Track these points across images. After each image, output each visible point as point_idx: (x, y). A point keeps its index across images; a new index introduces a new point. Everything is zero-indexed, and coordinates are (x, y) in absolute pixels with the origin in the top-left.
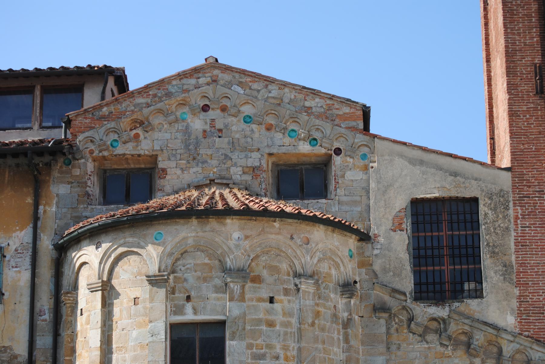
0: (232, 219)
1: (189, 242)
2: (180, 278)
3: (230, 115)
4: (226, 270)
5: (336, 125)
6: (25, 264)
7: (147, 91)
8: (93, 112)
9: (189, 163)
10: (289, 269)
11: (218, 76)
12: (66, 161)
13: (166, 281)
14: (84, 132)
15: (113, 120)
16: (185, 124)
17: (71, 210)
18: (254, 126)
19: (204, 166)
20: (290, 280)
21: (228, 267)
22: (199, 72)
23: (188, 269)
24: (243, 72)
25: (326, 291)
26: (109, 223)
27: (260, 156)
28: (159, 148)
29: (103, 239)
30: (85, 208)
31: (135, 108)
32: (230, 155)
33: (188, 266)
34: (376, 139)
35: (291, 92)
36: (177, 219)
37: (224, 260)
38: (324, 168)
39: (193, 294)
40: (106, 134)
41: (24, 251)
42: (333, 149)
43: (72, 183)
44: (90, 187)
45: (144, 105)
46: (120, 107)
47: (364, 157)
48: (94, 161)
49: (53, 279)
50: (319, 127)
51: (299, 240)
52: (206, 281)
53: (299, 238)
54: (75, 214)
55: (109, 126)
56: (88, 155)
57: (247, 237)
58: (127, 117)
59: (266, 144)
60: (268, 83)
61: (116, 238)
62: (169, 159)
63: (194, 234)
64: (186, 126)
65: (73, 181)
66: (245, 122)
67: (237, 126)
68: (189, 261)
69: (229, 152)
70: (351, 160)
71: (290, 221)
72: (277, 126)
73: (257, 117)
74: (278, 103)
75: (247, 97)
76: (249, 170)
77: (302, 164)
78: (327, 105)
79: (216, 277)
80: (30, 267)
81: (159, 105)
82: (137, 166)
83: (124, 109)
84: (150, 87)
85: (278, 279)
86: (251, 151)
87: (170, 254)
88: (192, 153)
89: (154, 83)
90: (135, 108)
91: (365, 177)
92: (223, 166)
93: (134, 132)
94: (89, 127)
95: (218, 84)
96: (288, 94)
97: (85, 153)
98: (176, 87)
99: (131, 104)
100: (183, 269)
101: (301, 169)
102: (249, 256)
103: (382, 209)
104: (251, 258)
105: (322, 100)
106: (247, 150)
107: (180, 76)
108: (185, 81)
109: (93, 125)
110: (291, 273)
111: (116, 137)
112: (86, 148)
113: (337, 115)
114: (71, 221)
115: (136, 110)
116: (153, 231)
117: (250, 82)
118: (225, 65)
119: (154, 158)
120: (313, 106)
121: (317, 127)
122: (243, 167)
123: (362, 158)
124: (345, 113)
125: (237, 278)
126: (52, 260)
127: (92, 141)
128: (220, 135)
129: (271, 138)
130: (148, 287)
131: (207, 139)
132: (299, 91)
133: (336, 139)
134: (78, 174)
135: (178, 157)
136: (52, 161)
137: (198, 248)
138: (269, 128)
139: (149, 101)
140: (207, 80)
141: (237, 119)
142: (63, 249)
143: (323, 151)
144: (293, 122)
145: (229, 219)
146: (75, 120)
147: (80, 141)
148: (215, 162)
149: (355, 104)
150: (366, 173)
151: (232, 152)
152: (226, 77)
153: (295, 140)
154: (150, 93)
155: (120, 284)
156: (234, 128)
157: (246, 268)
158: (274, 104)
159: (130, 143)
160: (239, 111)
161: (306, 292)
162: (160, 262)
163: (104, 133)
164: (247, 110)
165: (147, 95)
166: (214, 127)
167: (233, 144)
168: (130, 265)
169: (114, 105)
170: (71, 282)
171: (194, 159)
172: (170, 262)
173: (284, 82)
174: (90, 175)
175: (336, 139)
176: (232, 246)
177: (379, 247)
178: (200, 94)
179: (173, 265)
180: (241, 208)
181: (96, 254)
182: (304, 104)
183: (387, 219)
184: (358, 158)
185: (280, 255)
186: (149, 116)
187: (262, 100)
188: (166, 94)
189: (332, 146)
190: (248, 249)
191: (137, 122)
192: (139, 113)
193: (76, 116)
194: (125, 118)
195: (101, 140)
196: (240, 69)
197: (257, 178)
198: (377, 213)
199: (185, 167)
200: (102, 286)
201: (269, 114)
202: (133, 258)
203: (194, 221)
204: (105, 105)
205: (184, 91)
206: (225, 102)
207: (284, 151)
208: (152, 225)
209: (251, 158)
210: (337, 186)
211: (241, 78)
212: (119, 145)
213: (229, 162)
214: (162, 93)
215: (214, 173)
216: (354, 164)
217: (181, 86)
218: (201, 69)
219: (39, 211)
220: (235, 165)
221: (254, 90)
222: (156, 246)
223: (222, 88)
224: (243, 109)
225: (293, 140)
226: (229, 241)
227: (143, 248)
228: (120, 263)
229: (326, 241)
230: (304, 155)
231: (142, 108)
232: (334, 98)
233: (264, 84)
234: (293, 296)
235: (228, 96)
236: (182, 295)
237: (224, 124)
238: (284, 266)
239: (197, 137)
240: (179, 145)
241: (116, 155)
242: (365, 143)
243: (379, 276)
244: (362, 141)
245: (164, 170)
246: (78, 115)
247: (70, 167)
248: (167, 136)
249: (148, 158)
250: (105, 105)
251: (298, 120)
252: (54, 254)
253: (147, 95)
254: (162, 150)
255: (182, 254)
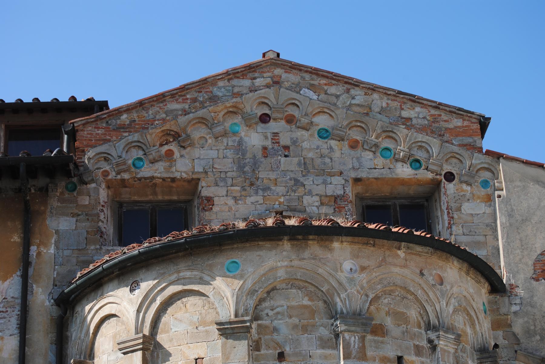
0: (342, 242)
1: (279, 275)
2: (266, 327)
3: (299, 127)
4: (333, 314)
5: (446, 142)
6: (10, 327)
7: (183, 93)
8: (107, 119)
9: (245, 190)
10: (420, 319)
11: (281, 77)
12: (70, 186)
13: (248, 329)
14: (95, 147)
15: (136, 132)
16: (237, 139)
17: (76, 252)
18: (333, 143)
19: (266, 194)
20: (421, 333)
21: (339, 309)
22: (255, 71)
23: (278, 313)
24: (316, 72)
25: (465, 355)
26: (156, 249)
27: (343, 182)
28: (201, 170)
29: (142, 276)
30: (97, 249)
31: (167, 116)
32: (302, 179)
33: (278, 309)
34: (501, 160)
35: (381, 99)
36: (261, 241)
37: (332, 299)
38: (426, 203)
39: (288, 349)
40: (126, 149)
41: (9, 309)
42: (443, 173)
43: (79, 215)
44: (103, 222)
45: (180, 113)
46: (146, 115)
47: (485, 184)
48: (108, 187)
49: (54, 347)
50: (423, 144)
51: (431, 278)
52: (307, 330)
53: (431, 275)
54: (82, 258)
55: (130, 138)
56: (101, 178)
57: (363, 269)
58: (155, 128)
59: (351, 167)
60: (349, 86)
61: (164, 273)
62: (217, 185)
63: (286, 263)
64: (239, 142)
65: (80, 213)
66: (320, 137)
67: (309, 143)
68: (280, 303)
69: (301, 175)
70: (469, 188)
71: (419, 248)
72: (364, 142)
73: (337, 130)
74: (365, 112)
75: (322, 105)
76: (330, 201)
77: (395, 198)
78: (432, 115)
79: (322, 325)
80: (16, 331)
81: (201, 113)
82: (167, 198)
83: (152, 116)
84: (188, 89)
85: (407, 332)
86: (331, 175)
87: (252, 292)
88: (248, 175)
89: (193, 83)
90: (167, 116)
91: (489, 210)
92: (293, 194)
93: (166, 148)
94: (103, 140)
95: (281, 87)
96: (378, 102)
97: (96, 176)
98: (223, 90)
99: (161, 111)
100: (271, 313)
101: (395, 205)
102: (367, 296)
103: (518, 251)
104: (370, 299)
105: (424, 110)
106: (325, 173)
107: (230, 75)
108: (235, 82)
109: (108, 137)
110: (422, 324)
111: (140, 153)
112: (98, 169)
113: (447, 129)
114: (77, 267)
115: (168, 118)
116: (223, 260)
117: (326, 85)
118: (291, 62)
119: (193, 183)
120: (412, 116)
121: (419, 144)
122: (321, 196)
123: (482, 186)
124: (456, 127)
125: (354, 325)
126: (52, 319)
127: (106, 159)
128: (286, 154)
129: (358, 159)
130: (220, 342)
131: (268, 159)
132: (393, 98)
133: (447, 161)
134: (87, 203)
135: (229, 182)
136: (50, 185)
137: (292, 282)
138: (354, 145)
139: (187, 107)
140: (266, 82)
141: (309, 133)
142: (68, 303)
143: (430, 176)
144: (385, 138)
145: (337, 241)
146: (82, 130)
147: (89, 159)
148: (281, 189)
149: (469, 115)
150: (490, 206)
151: (304, 176)
152: (293, 78)
153: (390, 160)
154: (188, 96)
155: (171, 340)
156: (305, 145)
157: (364, 312)
158: (359, 113)
159: (160, 163)
160: (312, 123)
161: (445, 351)
162: (237, 303)
163: (124, 149)
164: (323, 121)
165: (183, 99)
166: (278, 143)
167: (306, 166)
168: (187, 312)
169: (137, 112)
170: (84, 348)
171: (252, 184)
172: (251, 303)
173: (372, 85)
174: (103, 206)
175: (447, 161)
176: (344, 281)
177: (518, 301)
178: (256, 99)
179: (256, 308)
180: (356, 226)
181: (131, 300)
182: (400, 114)
183: (526, 264)
184: (477, 186)
185: (406, 298)
186: (186, 127)
187: (343, 108)
188: (210, 98)
189: (442, 169)
190: (365, 285)
191: (170, 134)
192: (172, 123)
193: (84, 124)
194: (153, 128)
195: (120, 157)
196: (311, 68)
197: (340, 211)
198: (511, 257)
199: (239, 195)
200: (143, 343)
201: (352, 127)
202: (191, 300)
203: (286, 245)
204: (125, 111)
205: (234, 94)
206: (292, 110)
207: (376, 175)
208: (221, 251)
209: (331, 184)
210: (452, 222)
211: (312, 80)
212: (145, 166)
213: (301, 189)
214: (204, 97)
215: (280, 203)
216: (472, 193)
217: (230, 88)
218: (257, 66)
219: (31, 253)
220: (310, 193)
221: (332, 95)
222: (229, 279)
223: (288, 91)
224: (316, 120)
225: (388, 161)
226: (339, 273)
227: (208, 283)
228: (170, 310)
229: (461, 284)
230: (403, 182)
231: (177, 116)
232: (441, 107)
233: (345, 88)
234: (427, 358)
235: (296, 102)
236: (271, 351)
237: (291, 139)
238: (413, 314)
239: (254, 156)
240: (230, 166)
241: (140, 179)
242: (486, 166)
243: (521, 341)
244: (482, 163)
245: (210, 200)
246: (87, 123)
247: (75, 193)
248: (213, 154)
249: (185, 184)
250: (125, 111)
251: (394, 135)
252: (55, 311)
253: (183, 99)
254: (206, 173)
255: (268, 293)
